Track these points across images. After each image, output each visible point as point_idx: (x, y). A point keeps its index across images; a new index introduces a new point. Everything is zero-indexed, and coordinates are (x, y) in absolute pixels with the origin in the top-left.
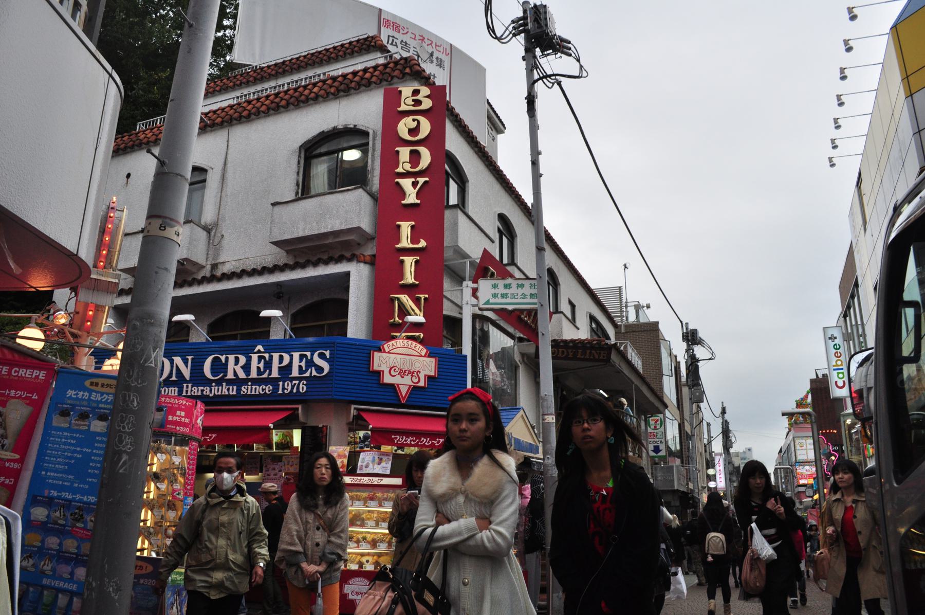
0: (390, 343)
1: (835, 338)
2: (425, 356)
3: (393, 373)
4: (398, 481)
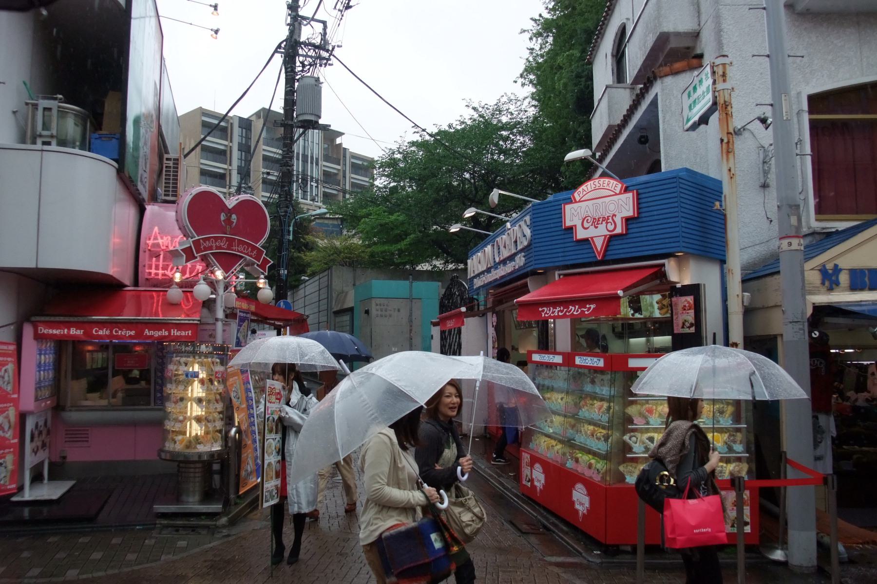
0: (580, 189)
1: (724, 81)
2: (620, 193)
3: (586, 225)
4: (654, 497)
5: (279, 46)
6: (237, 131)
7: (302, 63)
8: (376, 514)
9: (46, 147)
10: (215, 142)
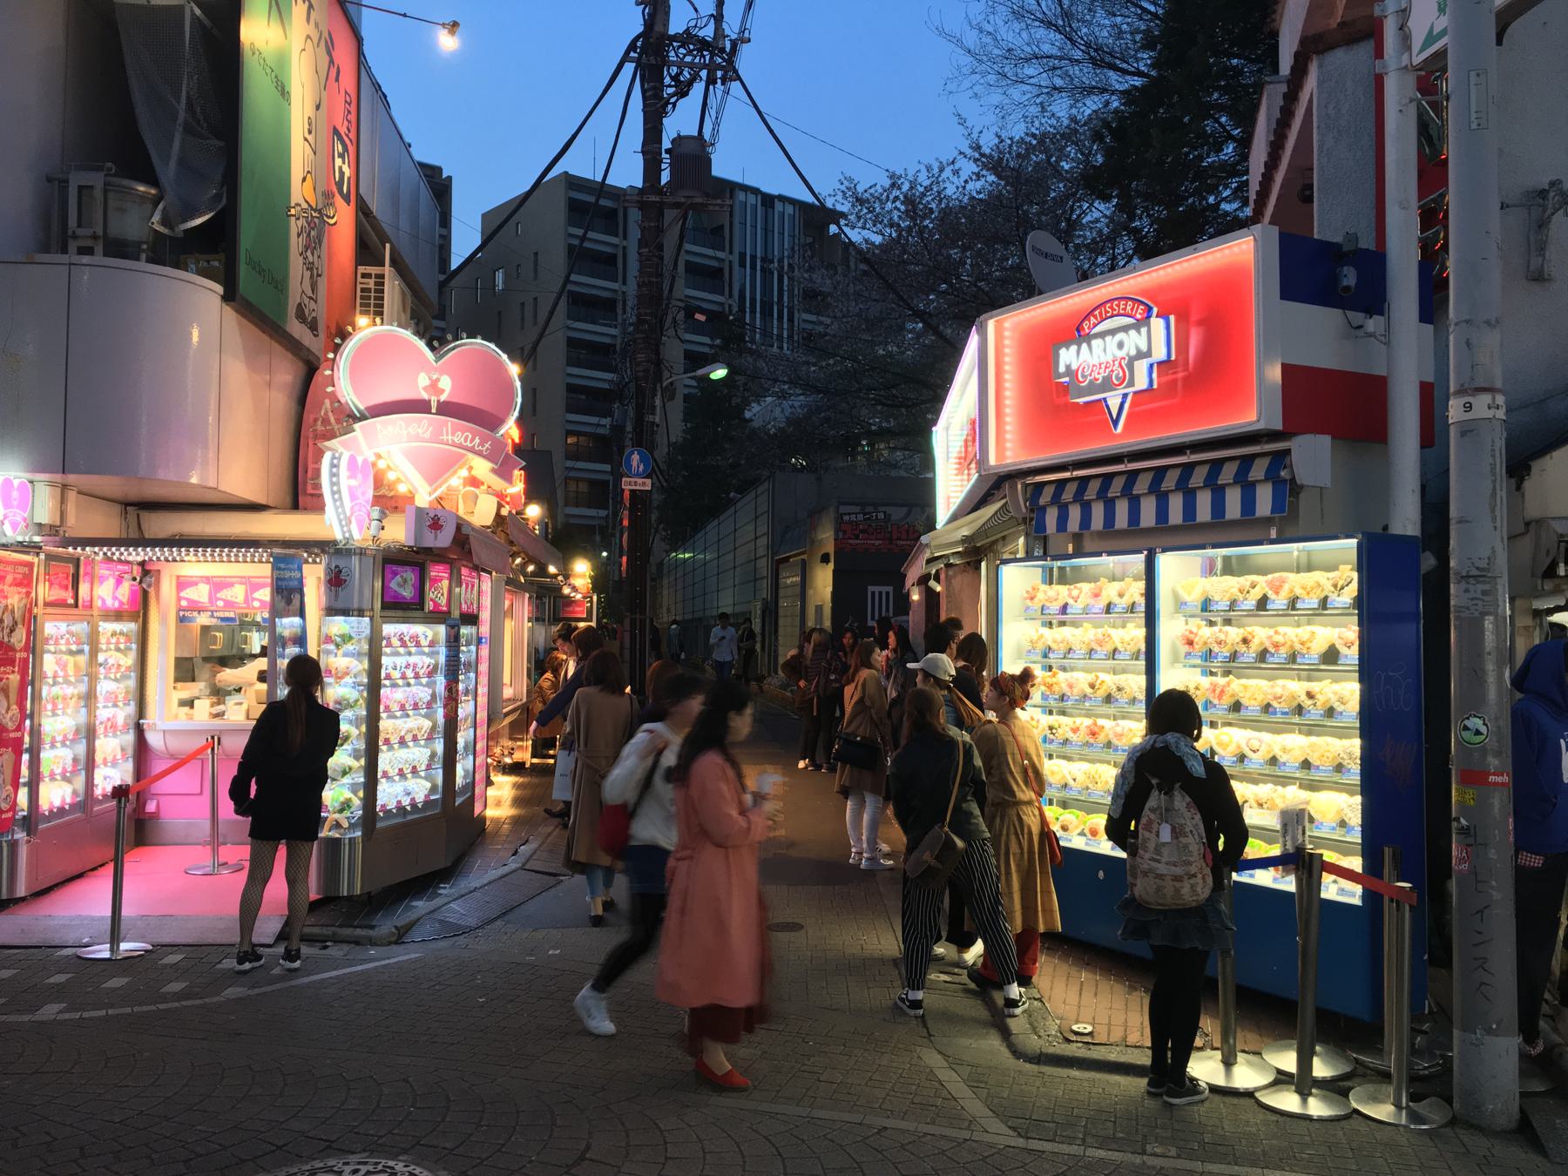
5: (632, 46)
6: (635, 215)
7: (675, 78)
8: (212, 705)
9: (85, 259)
10: (600, 240)
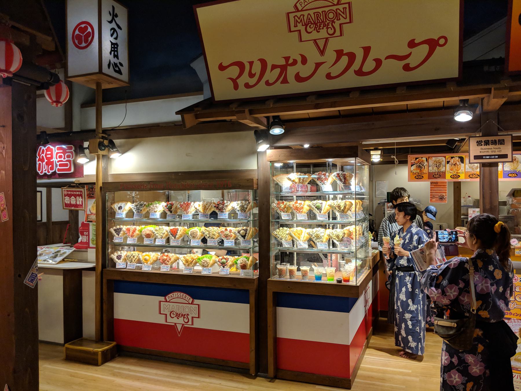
3: (172, 316)
